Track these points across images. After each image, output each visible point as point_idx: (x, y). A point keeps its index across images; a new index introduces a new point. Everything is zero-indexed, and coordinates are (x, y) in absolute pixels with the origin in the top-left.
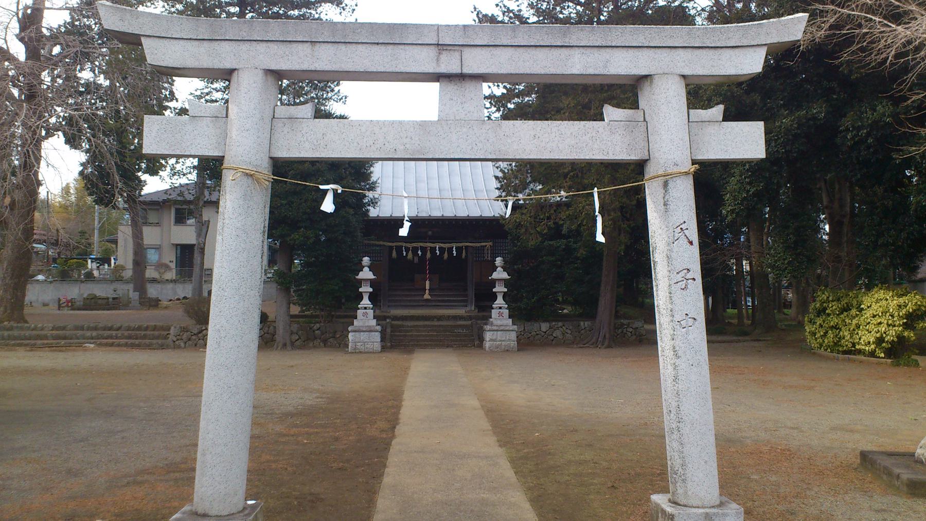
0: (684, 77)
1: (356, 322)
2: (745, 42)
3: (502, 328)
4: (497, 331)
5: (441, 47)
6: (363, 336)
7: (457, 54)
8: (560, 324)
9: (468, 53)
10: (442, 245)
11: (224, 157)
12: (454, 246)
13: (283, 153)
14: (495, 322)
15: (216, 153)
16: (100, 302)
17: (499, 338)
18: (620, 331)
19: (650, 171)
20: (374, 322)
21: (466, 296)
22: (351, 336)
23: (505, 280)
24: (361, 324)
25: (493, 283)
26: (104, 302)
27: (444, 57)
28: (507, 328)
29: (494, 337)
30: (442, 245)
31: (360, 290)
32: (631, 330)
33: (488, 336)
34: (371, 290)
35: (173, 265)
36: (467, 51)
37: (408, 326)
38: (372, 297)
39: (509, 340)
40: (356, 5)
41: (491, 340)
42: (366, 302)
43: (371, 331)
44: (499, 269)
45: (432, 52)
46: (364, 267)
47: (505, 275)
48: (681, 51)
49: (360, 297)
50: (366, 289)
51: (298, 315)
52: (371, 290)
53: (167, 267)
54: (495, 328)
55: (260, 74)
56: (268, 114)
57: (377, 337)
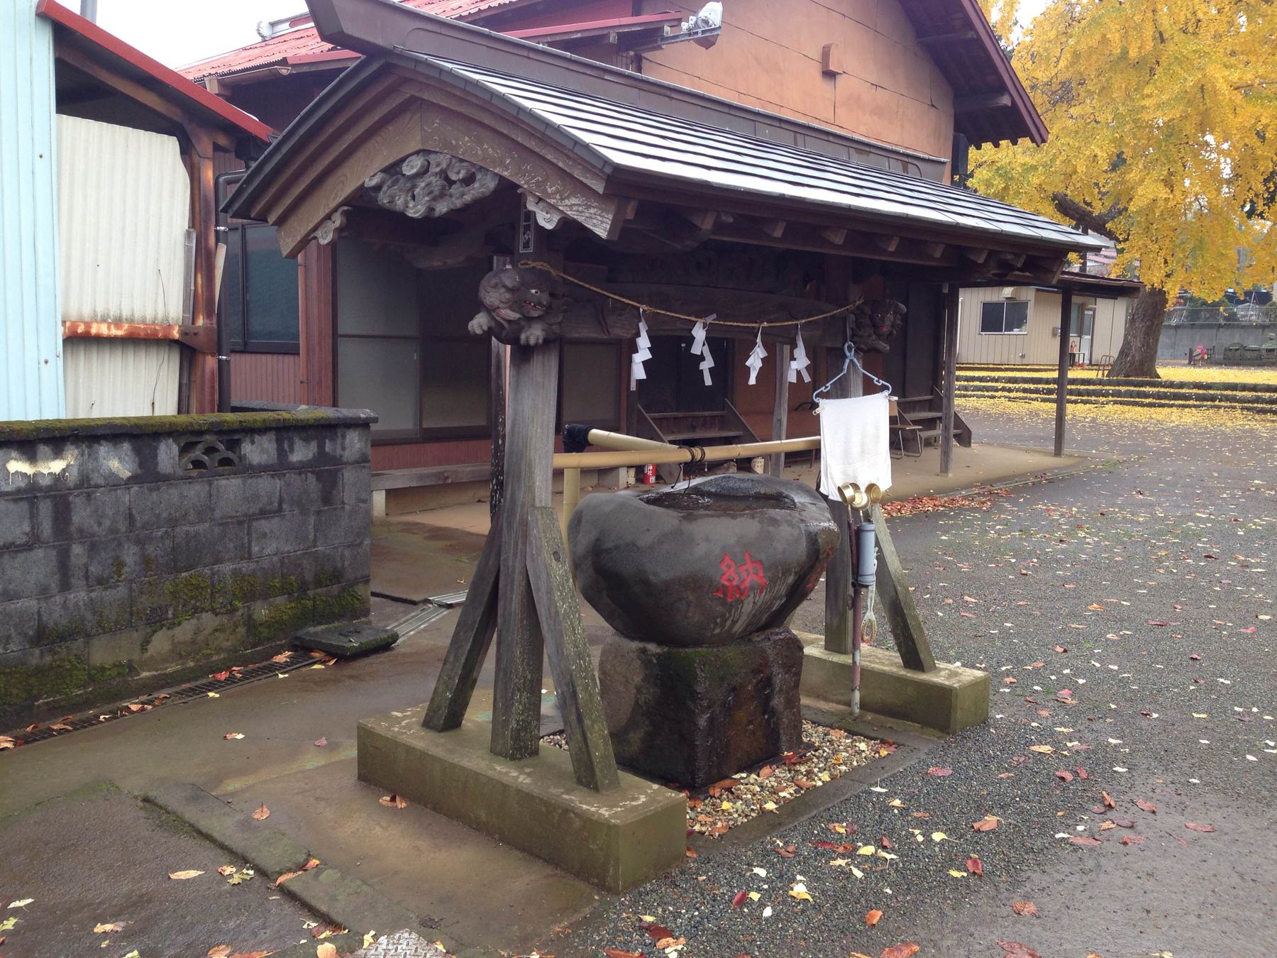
16: (1248, 355)
26: (1254, 354)
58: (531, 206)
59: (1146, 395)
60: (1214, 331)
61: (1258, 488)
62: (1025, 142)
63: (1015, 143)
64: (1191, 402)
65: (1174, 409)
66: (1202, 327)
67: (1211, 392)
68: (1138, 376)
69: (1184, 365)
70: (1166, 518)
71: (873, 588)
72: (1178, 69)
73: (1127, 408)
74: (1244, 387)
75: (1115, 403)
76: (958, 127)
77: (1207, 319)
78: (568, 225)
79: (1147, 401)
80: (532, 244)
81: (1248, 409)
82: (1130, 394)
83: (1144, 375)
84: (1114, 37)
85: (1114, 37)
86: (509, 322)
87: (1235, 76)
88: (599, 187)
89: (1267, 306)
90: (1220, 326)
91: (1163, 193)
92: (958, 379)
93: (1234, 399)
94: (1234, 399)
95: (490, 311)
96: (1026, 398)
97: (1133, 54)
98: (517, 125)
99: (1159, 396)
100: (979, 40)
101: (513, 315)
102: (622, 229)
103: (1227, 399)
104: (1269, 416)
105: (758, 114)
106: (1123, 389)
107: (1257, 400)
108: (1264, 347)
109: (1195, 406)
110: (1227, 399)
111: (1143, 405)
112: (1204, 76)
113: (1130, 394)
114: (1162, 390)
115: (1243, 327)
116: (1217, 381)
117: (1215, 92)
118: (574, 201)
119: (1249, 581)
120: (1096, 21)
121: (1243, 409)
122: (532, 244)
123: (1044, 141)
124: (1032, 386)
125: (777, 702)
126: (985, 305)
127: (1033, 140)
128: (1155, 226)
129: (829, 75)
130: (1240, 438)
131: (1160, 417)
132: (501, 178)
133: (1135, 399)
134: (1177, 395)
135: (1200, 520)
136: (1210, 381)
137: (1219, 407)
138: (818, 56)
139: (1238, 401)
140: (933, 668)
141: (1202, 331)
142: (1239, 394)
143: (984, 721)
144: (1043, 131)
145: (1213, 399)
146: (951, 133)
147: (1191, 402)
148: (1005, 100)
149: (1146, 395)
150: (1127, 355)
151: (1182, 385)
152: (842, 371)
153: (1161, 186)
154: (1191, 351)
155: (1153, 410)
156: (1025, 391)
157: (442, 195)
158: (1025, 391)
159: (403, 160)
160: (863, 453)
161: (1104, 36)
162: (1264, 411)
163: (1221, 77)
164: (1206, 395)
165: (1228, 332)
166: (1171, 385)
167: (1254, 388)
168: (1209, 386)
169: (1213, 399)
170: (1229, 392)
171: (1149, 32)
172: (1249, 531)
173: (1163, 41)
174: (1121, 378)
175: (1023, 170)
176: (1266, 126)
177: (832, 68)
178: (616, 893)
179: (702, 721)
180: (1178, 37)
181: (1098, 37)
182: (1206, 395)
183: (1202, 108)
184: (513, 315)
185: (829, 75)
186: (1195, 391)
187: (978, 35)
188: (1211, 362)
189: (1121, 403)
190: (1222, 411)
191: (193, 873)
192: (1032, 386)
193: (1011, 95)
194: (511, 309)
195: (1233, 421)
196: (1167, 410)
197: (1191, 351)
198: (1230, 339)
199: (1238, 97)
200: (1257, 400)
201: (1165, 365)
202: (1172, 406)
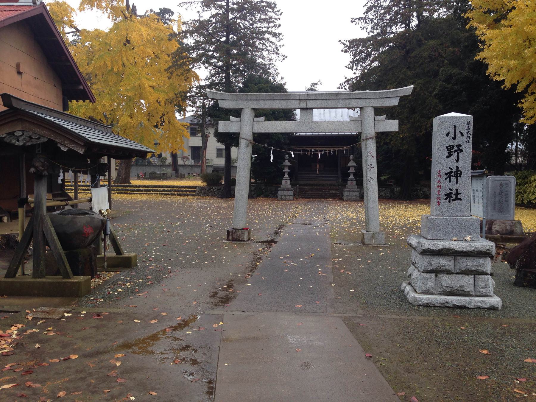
0: (373, 107)
1: (281, 186)
2: (392, 96)
3: (352, 190)
4: (350, 191)
5: (300, 100)
6: (285, 192)
7: (305, 102)
8: (384, 189)
9: (308, 102)
10: (326, 149)
11: (240, 133)
12: (332, 149)
13: (255, 131)
14: (349, 187)
15: (238, 132)
16: (157, 175)
17: (351, 195)
18: (415, 193)
19: (363, 137)
20: (290, 186)
21: (337, 174)
22: (279, 192)
23: (354, 166)
24: (284, 187)
25: (349, 168)
26: (159, 175)
27: (302, 103)
28: (355, 190)
29: (348, 194)
30: (326, 149)
31: (284, 171)
32: (421, 192)
33: (346, 193)
34: (289, 171)
35: (190, 157)
36: (308, 101)
37: (307, 189)
38: (289, 174)
39: (356, 196)
40: (282, 39)
41: (347, 196)
42: (286, 176)
43: (288, 190)
44: (351, 161)
45: (298, 102)
46: (285, 160)
47: (354, 164)
48: (372, 99)
49: (284, 174)
50: (286, 170)
51: (337, 94)
52: (289, 171)
53: (187, 158)
54: (349, 190)
55: (250, 109)
56: (252, 121)
57: (291, 193)
58: (59, 145)
59: (128, 190)
60: (144, 167)
61: (173, 216)
62: (87, 101)
63: (84, 101)
64: (143, 192)
65: (138, 195)
66: (140, 166)
67: (150, 188)
68: (125, 183)
69: (136, 180)
70: (153, 224)
71: (109, 235)
72: (131, 77)
73: (122, 195)
74: (159, 187)
75: (118, 193)
76: (64, 94)
77: (141, 163)
78: (70, 150)
79: (129, 192)
80: (41, 151)
81: (162, 194)
82: (123, 190)
83: (126, 183)
84: (109, 64)
85: (109, 64)
86: (41, 170)
87: (151, 84)
88: (82, 144)
89: (161, 158)
90: (146, 166)
91: (130, 120)
92: (67, 186)
93: (156, 191)
94: (156, 191)
95: (35, 167)
96: (84, 193)
97: (115, 70)
98: (41, 126)
99: (132, 190)
100: (72, 66)
101: (43, 169)
102: (85, 152)
103: (155, 191)
104: (168, 196)
105: (79, 118)
106: (120, 188)
107: (164, 191)
108: (162, 173)
109: (145, 194)
110: (155, 191)
111: (127, 194)
112: (141, 82)
113: (123, 190)
114: (133, 188)
115: (154, 166)
116: (150, 185)
117: (144, 88)
118: (73, 146)
119: (181, 236)
120: (101, 57)
121: (160, 194)
122: (41, 151)
123: (95, 102)
124: (86, 188)
125: (93, 263)
126: (383, 198)
127: (91, 101)
128: (127, 131)
129: (19, 73)
130: (162, 203)
131: (135, 198)
132: (49, 139)
133: (125, 192)
134: (138, 190)
135: (162, 224)
136: (148, 185)
137: (152, 194)
138: (15, 66)
139: (158, 191)
140: (124, 254)
141: (140, 167)
142: (158, 189)
143: (136, 265)
144: (94, 98)
145: (150, 191)
146: (62, 96)
147: (143, 192)
148: (81, 87)
149: (128, 190)
150: (120, 176)
151: (139, 186)
152: (96, 181)
153: (129, 118)
154: (138, 175)
155: (131, 195)
156: (83, 190)
157: (28, 141)
158: (83, 190)
159: (15, 131)
160: (102, 202)
161: (105, 62)
162: (166, 194)
163: (147, 84)
164: (148, 190)
165: (149, 168)
166: (136, 186)
167: (162, 187)
168: (148, 187)
169: (150, 191)
170: (155, 188)
171: (120, 63)
172: (175, 226)
173: (125, 66)
174: (118, 184)
175: (77, 106)
176: (161, 101)
177: (21, 71)
178: (81, 297)
179: (80, 267)
180: (130, 66)
181: (103, 62)
182: (148, 190)
183: (140, 92)
184: (43, 169)
185: (19, 73)
186: (144, 188)
187: (71, 64)
188: (145, 178)
189: (120, 193)
190: (153, 195)
191: (272, 158)
192: (86, 188)
193: (83, 86)
194: (42, 167)
195: (158, 198)
196: (136, 195)
197: (138, 175)
198: (149, 170)
199: (152, 90)
200: (164, 191)
201: (133, 180)
202: (137, 194)
